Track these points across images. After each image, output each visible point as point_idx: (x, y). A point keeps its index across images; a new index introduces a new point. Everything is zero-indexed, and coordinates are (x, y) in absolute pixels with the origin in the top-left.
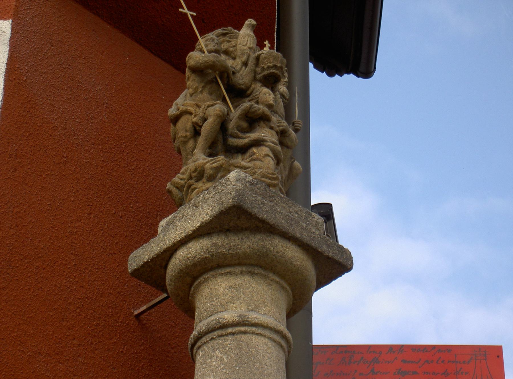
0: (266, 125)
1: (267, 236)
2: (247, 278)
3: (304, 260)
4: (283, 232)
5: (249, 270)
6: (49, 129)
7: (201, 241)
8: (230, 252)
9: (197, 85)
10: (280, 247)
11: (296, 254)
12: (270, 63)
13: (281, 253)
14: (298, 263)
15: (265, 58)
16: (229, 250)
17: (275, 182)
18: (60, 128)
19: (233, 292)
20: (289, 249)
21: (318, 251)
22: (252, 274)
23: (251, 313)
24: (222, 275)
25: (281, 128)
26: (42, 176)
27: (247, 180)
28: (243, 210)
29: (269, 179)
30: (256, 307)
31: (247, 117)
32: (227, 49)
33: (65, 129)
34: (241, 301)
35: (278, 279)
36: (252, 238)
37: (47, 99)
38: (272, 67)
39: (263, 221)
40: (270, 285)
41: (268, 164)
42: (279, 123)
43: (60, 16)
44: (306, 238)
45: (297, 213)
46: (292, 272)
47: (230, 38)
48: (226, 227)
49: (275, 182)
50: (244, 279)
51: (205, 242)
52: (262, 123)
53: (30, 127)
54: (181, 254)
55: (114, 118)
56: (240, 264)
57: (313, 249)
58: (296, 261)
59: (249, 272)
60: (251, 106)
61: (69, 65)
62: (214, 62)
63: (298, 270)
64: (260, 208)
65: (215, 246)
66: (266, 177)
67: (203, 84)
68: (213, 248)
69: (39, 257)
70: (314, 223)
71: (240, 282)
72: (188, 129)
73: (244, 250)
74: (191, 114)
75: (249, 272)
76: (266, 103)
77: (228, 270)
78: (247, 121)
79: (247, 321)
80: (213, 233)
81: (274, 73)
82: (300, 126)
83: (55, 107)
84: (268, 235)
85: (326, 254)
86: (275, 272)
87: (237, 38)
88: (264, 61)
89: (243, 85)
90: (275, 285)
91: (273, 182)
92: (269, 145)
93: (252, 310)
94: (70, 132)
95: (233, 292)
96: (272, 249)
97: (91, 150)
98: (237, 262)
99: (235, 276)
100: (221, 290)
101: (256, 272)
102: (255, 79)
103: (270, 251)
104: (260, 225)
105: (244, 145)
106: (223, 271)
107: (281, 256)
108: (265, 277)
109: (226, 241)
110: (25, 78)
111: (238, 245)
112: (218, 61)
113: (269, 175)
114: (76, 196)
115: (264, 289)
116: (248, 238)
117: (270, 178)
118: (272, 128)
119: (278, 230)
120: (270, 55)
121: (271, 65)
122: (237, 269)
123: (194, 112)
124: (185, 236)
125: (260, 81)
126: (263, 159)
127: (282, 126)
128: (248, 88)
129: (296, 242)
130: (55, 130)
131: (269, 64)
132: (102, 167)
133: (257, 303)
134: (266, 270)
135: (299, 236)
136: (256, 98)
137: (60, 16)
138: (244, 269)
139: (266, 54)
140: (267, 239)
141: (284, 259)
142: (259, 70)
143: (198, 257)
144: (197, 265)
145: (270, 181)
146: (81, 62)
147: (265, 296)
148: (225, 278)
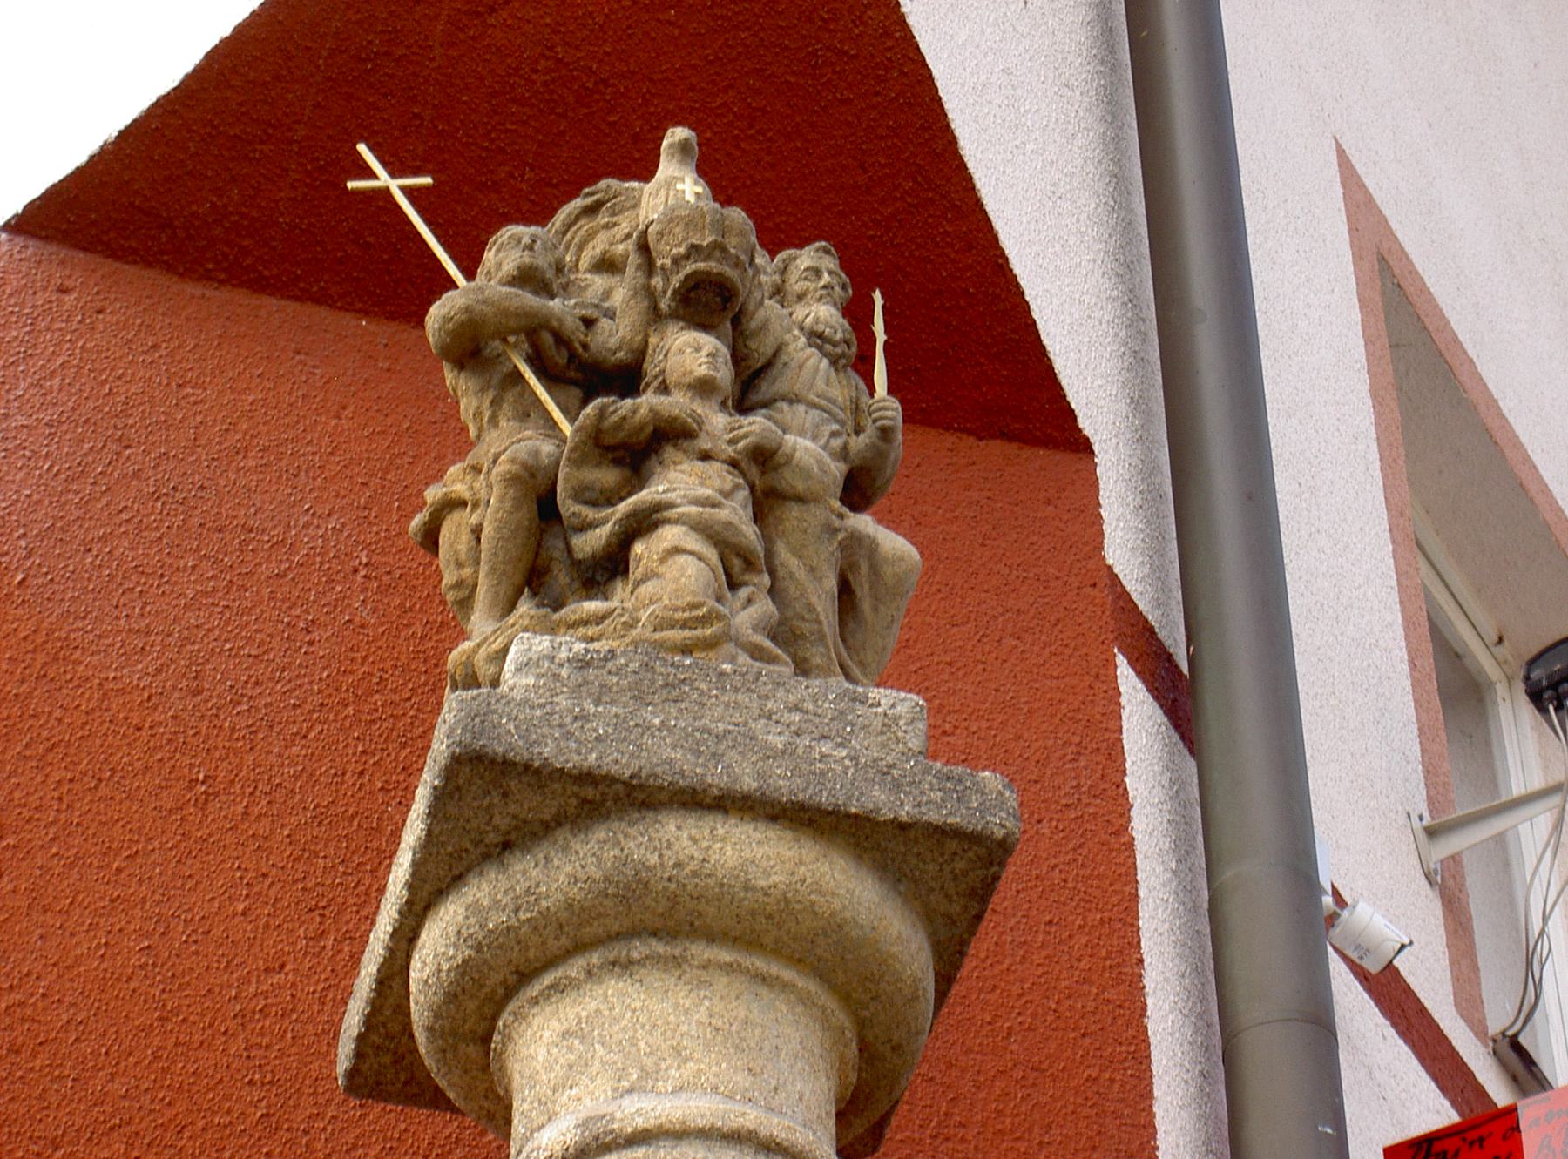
0: (685, 452)
1: (632, 823)
2: (613, 986)
3: (801, 863)
4: (682, 791)
5: (611, 957)
6: (131, 710)
7: (442, 910)
8: (522, 916)
9: (475, 404)
10: (686, 843)
11: (760, 852)
12: (680, 245)
13: (692, 866)
14: (776, 879)
15: (661, 234)
16: (517, 911)
17: (708, 632)
18: (177, 695)
19: (570, 1049)
20: (723, 840)
21: (848, 815)
22: (625, 966)
23: (626, 1101)
24: (535, 1001)
25: (741, 445)
26: (109, 865)
27: (563, 654)
28: (493, 761)
29: (683, 627)
30: (645, 1074)
31: (608, 448)
32: (605, 253)
33: (199, 692)
34: (594, 1070)
35: (726, 956)
36: (578, 846)
37: (117, 618)
38: (687, 257)
39: (587, 777)
40: (701, 983)
41: (676, 580)
42: (733, 429)
43: (155, 347)
44: (785, 783)
45: (796, 708)
46: (770, 917)
47: (614, 214)
48: (492, 838)
49: (708, 632)
50: (605, 993)
51: (452, 908)
52: (669, 453)
53: (52, 722)
54: (419, 971)
55: (402, 605)
56: (580, 947)
57: (830, 813)
58: (766, 873)
59: (614, 964)
60: (602, 413)
61: (202, 488)
62: (467, 310)
63: (787, 901)
64: (569, 735)
65: (474, 913)
66: (672, 626)
67: (491, 394)
68: (472, 920)
69: (112, 1129)
70: (877, 724)
71: (593, 1005)
72: (463, 556)
73: (560, 896)
74: (464, 504)
75: (614, 964)
76: (687, 380)
77: (548, 979)
78: (617, 462)
79: (606, 1134)
80: (469, 869)
81: (695, 273)
82: (889, 413)
83: (148, 634)
84: (637, 815)
85: (886, 814)
86: (711, 938)
87: (636, 206)
88: (661, 247)
89: (620, 348)
90: (725, 980)
91: (699, 632)
92: (688, 515)
93: (630, 1091)
94: (219, 696)
95: (570, 1049)
96: (654, 859)
97: (309, 730)
98: (564, 941)
99: (575, 993)
100: (542, 1052)
101: (635, 955)
102: (655, 317)
103: (649, 869)
104: (590, 792)
105: (609, 544)
106: (534, 989)
107: (695, 874)
108: (677, 962)
109: (504, 884)
110: (20, 577)
111: (538, 886)
112: (484, 302)
113: (679, 615)
114: (259, 894)
115: (677, 1005)
116: (565, 849)
117: (684, 625)
118: (705, 456)
119: (661, 788)
120: (671, 220)
121: (682, 250)
122: (573, 969)
123: (467, 495)
124: (400, 913)
125: (675, 316)
126: (662, 569)
127: (745, 436)
128: (641, 353)
129: (751, 808)
130: (155, 707)
131: (674, 251)
132: (362, 773)
133: (649, 1062)
134: (675, 938)
135: (755, 785)
136: (656, 377)
137: (155, 347)
138: (595, 958)
139: (660, 221)
140: (632, 831)
141: (711, 882)
142: (657, 282)
143: (445, 967)
144: (456, 995)
145: (687, 633)
146: (252, 463)
147: (685, 1028)
148: (548, 1009)
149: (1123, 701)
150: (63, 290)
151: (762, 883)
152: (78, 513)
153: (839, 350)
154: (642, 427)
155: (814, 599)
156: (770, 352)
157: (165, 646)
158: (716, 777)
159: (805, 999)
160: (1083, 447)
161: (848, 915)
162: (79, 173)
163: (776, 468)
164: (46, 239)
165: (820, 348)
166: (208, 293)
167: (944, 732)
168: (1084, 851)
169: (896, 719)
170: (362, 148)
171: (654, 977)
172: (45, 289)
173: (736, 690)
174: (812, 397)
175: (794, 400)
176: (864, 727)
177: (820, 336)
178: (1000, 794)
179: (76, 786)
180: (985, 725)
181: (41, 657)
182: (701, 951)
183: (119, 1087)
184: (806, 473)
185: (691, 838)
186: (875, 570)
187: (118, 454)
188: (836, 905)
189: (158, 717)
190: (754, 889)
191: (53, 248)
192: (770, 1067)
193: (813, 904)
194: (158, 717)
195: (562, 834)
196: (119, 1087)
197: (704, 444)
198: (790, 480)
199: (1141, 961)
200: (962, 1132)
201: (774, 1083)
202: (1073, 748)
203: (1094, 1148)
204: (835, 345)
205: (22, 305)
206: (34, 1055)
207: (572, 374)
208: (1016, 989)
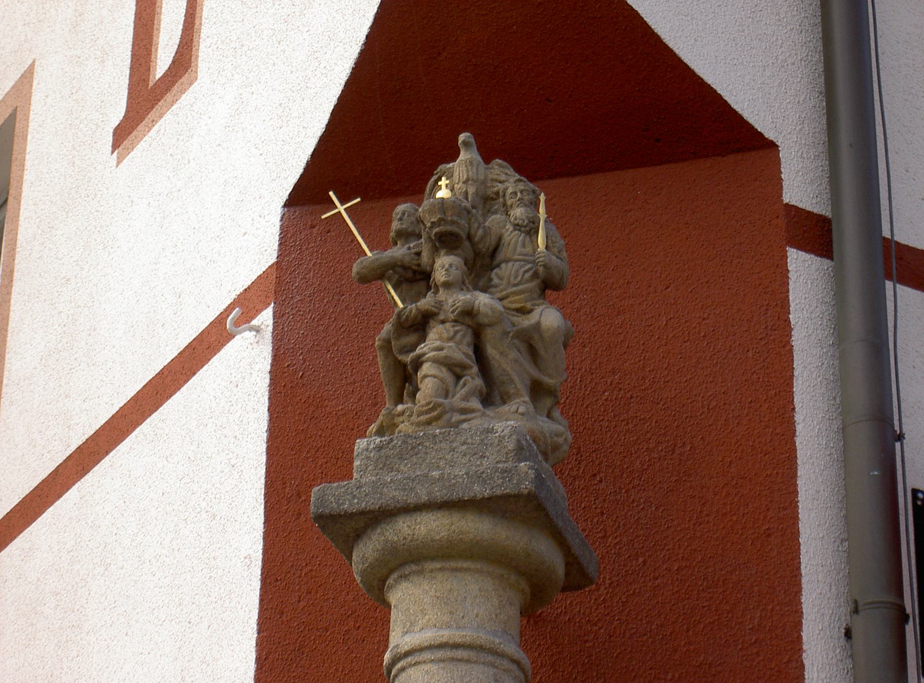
11: (434, 525)
17: (435, 413)
22: (405, 577)
33: (376, 404)
39: (362, 513)
44: (439, 494)
45: (464, 443)
49: (435, 413)
86: (433, 559)
90: (441, 574)
96: (396, 539)
107: (411, 541)
108: (420, 572)
117: (427, 412)
118: (443, 322)
145: (428, 416)
149: (790, 275)
150: (313, 227)
151: (438, 537)
152: (324, 335)
153: (528, 228)
154: (416, 317)
155: (505, 366)
156: (494, 243)
157: (362, 387)
158: (412, 500)
159: (477, 571)
160: (772, 146)
161: (478, 538)
162: (302, 176)
163: (476, 315)
164: (304, 204)
165: (520, 230)
166: (374, 205)
167: (704, 319)
168: (768, 360)
169: (504, 437)
170: (331, 193)
171: (415, 579)
172: (304, 229)
173: (441, 442)
174: (516, 257)
175: (507, 261)
176: (491, 444)
177: (518, 225)
178: (527, 473)
179: (329, 464)
180: (722, 309)
181: (312, 409)
182: (429, 565)
183: (350, 597)
184: (486, 315)
185: (408, 526)
186: (541, 337)
187: (339, 300)
188: (471, 536)
189: (360, 422)
190: (435, 540)
191: (306, 208)
192: (460, 607)
193: (461, 539)
194: (360, 422)
195: (369, 531)
196: (350, 597)
197: (442, 317)
198: (483, 320)
199: (794, 409)
200: (707, 519)
201: (462, 614)
202: (765, 308)
203: (768, 510)
204: (525, 227)
205: (295, 241)
206: (317, 592)
207: (419, 277)
208: (734, 441)
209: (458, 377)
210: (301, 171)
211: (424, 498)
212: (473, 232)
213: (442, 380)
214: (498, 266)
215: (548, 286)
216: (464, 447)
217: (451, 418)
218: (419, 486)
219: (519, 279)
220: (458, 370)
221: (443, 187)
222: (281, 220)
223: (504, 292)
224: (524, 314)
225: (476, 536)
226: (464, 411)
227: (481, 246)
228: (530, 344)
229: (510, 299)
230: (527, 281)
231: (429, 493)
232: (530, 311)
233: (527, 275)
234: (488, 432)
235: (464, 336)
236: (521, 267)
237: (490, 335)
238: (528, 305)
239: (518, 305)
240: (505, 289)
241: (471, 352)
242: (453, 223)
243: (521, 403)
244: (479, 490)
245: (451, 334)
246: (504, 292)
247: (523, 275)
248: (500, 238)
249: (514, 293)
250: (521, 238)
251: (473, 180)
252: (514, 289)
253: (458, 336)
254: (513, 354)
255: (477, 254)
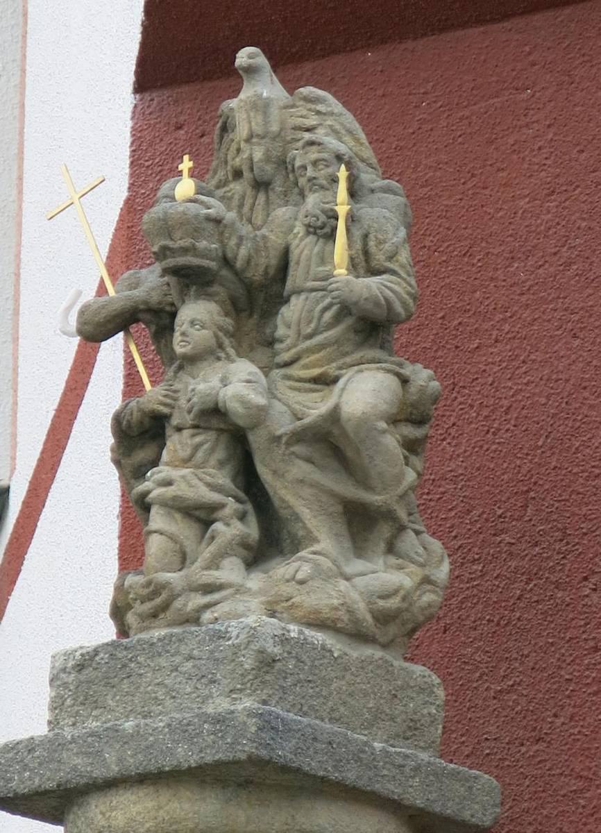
44: (134, 762)
45: (190, 657)
158: (99, 773)
165: (315, 233)
174: (310, 284)
191: (166, 93)
209: (206, 524)
210: (138, 37)
211: (114, 770)
212: (230, 255)
213: (172, 538)
214: (287, 301)
215: (370, 328)
216: (190, 664)
217: (185, 605)
218: (107, 749)
219: (313, 325)
220: (202, 514)
221: (185, 173)
222: (132, 118)
223: (293, 351)
224: (327, 384)
225: (198, 824)
226: (209, 589)
227: (249, 275)
228: (329, 441)
229: (302, 362)
230: (330, 326)
231: (120, 760)
232: (335, 380)
233: (328, 316)
234: (220, 637)
235: (212, 450)
236: (318, 302)
237: (256, 440)
238: (331, 369)
239: (316, 372)
240: (295, 346)
241: (223, 478)
242: (185, 251)
243: (325, 543)
244: (186, 755)
245: (188, 451)
246: (293, 351)
247: (320, 319)
248: (286, 253)
249: (310, 351)
250: (316, 249)
251: (258, 136)
252: (308, 343)
253: (200, 455)
254: (300, 469)
255: (249, 288)
